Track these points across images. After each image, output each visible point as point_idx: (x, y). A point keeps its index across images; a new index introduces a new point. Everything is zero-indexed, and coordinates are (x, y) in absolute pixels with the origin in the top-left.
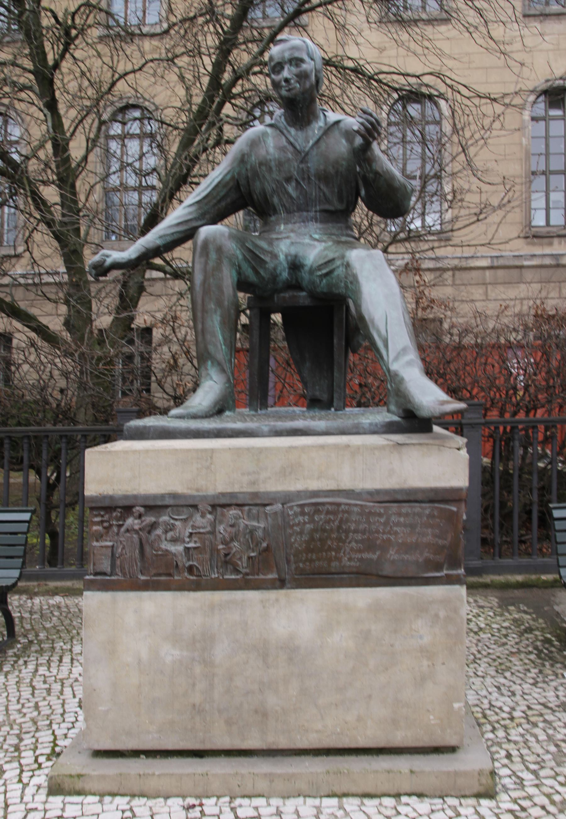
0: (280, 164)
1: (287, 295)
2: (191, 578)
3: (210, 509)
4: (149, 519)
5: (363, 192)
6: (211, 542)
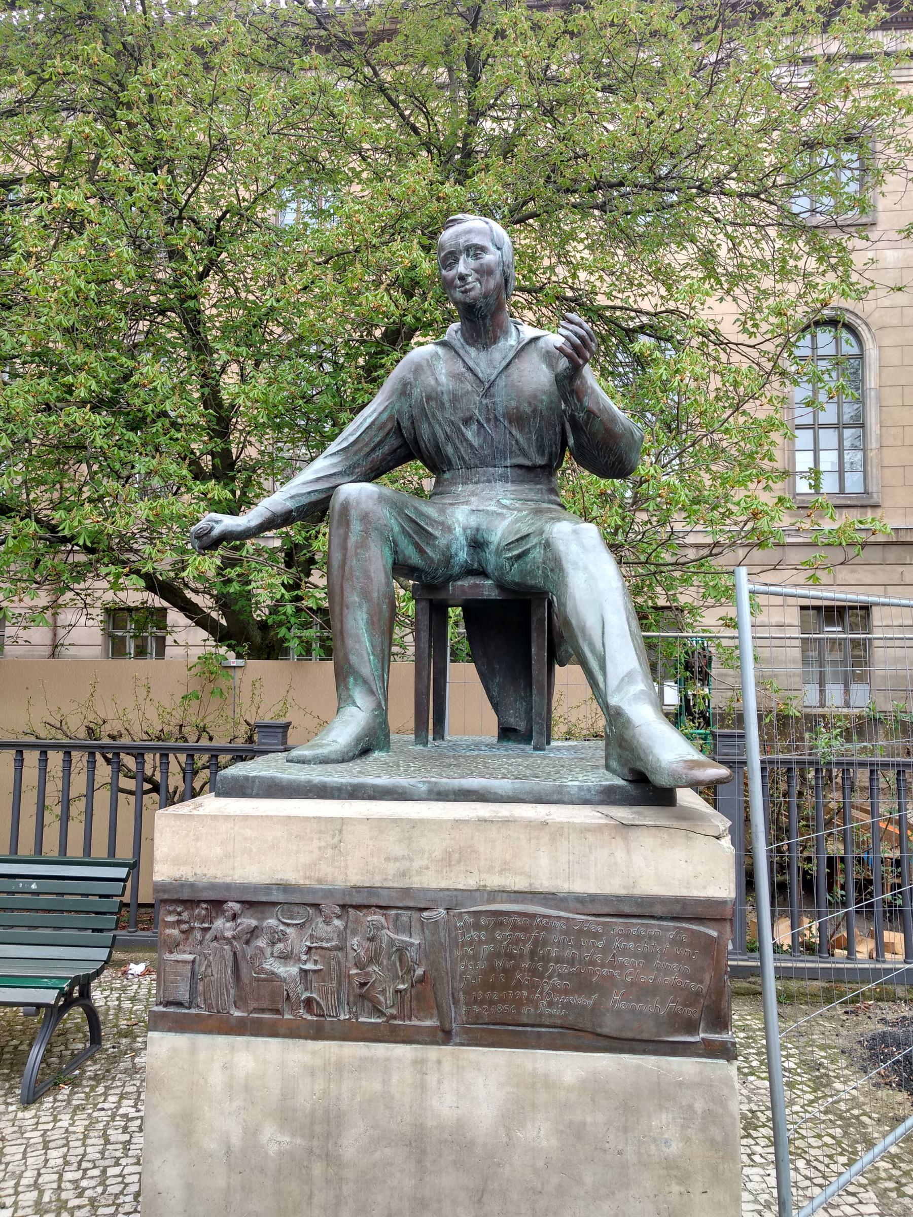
0: (455, 399)
1: (467, 582)
2: (310, 1018)
3: (338, 910)
4: (248, 921)
5: (571, 441)
6: (339, 963)
